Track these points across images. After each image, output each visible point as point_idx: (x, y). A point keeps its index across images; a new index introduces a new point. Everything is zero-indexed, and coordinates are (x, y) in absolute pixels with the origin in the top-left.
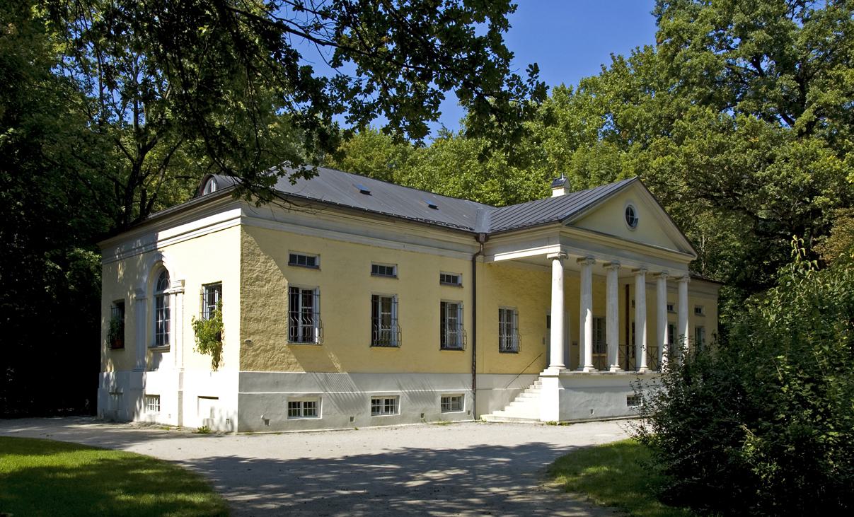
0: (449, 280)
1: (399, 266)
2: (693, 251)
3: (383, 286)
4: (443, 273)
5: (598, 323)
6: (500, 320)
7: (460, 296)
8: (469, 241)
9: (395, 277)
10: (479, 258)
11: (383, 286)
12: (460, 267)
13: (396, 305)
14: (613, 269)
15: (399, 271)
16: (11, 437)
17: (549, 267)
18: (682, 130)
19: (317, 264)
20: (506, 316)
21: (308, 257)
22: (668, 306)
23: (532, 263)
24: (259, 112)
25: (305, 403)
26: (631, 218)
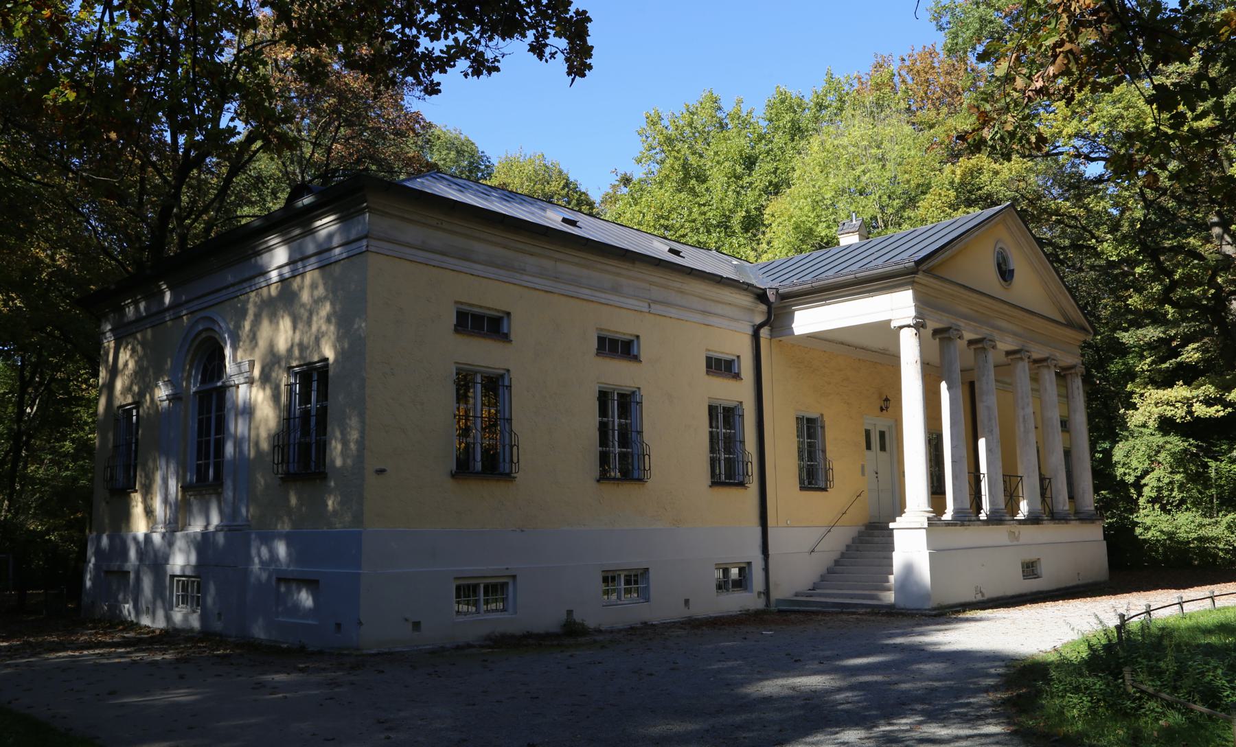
0: (721, 367)
1: (642, 339)
2: (1087, 325)
3: (619, 374)
4: (604, 334)
5: (808, 428)
6: (711, 426)
7: (738, 392)
8: (745, 300)
9: (636, 358)
10: (764, 332)
11: (619, 374)
12: (737, 345)
13: (506, 392)
14: (1021, 359)
15: (517, 328)
16: (802, 676)
17: (893, 355)
18: (886, 103)
19: (506, 331)
20: (810, 429)
21: (622, 341)
22: (1061, 422)
23: (826, 340)
24: (739, 178)
25: (486, 587)
26: (1006, 274)
